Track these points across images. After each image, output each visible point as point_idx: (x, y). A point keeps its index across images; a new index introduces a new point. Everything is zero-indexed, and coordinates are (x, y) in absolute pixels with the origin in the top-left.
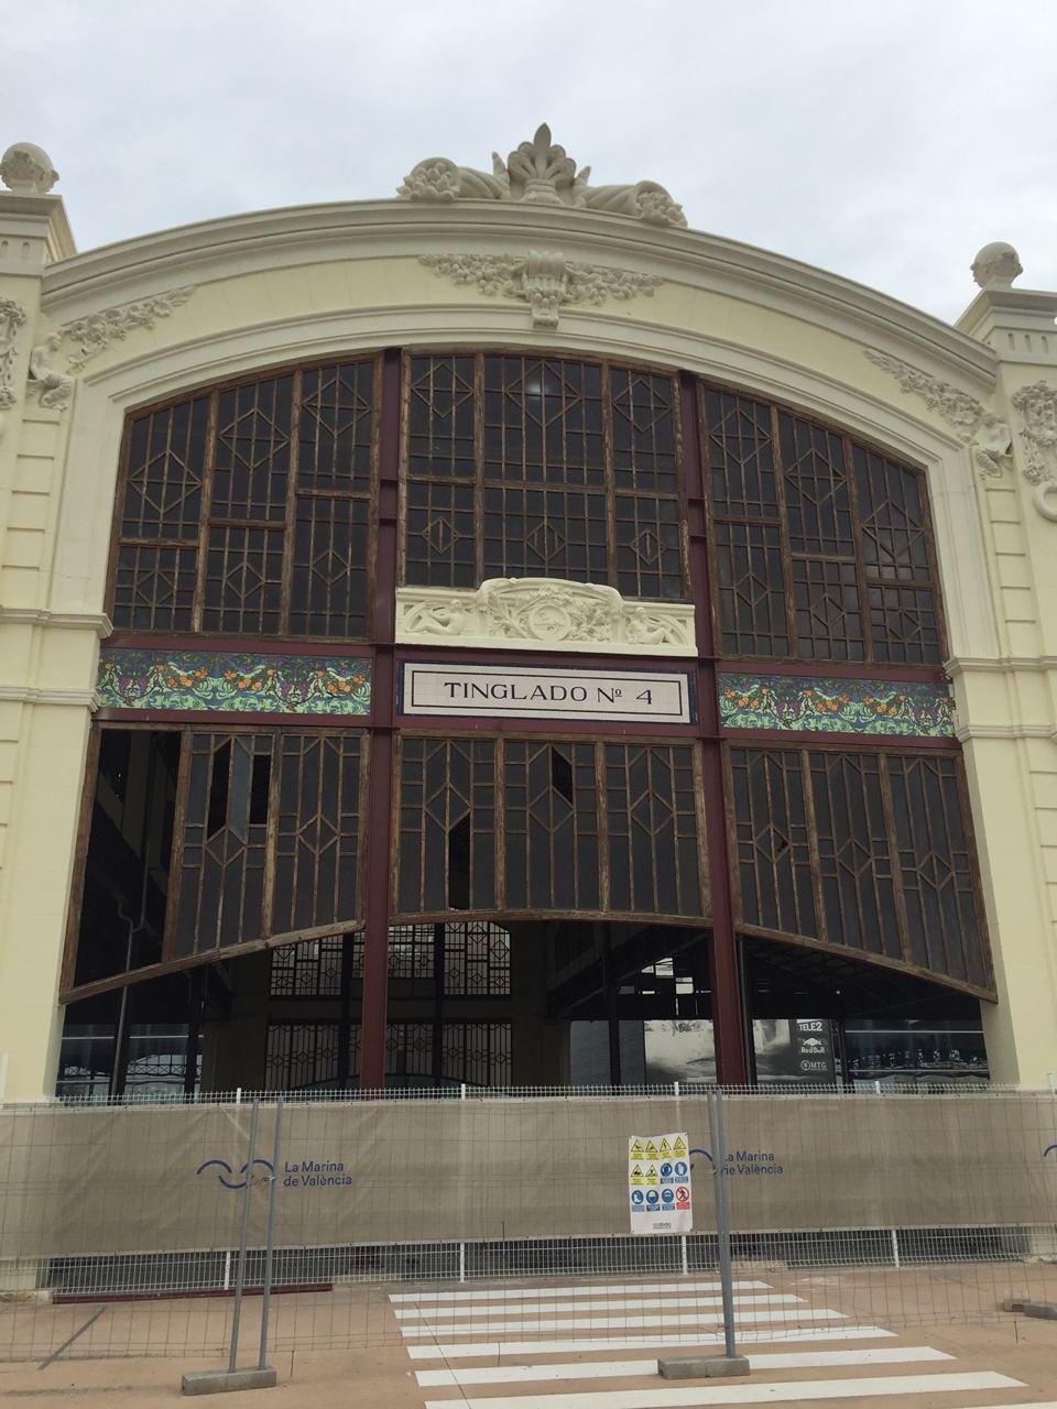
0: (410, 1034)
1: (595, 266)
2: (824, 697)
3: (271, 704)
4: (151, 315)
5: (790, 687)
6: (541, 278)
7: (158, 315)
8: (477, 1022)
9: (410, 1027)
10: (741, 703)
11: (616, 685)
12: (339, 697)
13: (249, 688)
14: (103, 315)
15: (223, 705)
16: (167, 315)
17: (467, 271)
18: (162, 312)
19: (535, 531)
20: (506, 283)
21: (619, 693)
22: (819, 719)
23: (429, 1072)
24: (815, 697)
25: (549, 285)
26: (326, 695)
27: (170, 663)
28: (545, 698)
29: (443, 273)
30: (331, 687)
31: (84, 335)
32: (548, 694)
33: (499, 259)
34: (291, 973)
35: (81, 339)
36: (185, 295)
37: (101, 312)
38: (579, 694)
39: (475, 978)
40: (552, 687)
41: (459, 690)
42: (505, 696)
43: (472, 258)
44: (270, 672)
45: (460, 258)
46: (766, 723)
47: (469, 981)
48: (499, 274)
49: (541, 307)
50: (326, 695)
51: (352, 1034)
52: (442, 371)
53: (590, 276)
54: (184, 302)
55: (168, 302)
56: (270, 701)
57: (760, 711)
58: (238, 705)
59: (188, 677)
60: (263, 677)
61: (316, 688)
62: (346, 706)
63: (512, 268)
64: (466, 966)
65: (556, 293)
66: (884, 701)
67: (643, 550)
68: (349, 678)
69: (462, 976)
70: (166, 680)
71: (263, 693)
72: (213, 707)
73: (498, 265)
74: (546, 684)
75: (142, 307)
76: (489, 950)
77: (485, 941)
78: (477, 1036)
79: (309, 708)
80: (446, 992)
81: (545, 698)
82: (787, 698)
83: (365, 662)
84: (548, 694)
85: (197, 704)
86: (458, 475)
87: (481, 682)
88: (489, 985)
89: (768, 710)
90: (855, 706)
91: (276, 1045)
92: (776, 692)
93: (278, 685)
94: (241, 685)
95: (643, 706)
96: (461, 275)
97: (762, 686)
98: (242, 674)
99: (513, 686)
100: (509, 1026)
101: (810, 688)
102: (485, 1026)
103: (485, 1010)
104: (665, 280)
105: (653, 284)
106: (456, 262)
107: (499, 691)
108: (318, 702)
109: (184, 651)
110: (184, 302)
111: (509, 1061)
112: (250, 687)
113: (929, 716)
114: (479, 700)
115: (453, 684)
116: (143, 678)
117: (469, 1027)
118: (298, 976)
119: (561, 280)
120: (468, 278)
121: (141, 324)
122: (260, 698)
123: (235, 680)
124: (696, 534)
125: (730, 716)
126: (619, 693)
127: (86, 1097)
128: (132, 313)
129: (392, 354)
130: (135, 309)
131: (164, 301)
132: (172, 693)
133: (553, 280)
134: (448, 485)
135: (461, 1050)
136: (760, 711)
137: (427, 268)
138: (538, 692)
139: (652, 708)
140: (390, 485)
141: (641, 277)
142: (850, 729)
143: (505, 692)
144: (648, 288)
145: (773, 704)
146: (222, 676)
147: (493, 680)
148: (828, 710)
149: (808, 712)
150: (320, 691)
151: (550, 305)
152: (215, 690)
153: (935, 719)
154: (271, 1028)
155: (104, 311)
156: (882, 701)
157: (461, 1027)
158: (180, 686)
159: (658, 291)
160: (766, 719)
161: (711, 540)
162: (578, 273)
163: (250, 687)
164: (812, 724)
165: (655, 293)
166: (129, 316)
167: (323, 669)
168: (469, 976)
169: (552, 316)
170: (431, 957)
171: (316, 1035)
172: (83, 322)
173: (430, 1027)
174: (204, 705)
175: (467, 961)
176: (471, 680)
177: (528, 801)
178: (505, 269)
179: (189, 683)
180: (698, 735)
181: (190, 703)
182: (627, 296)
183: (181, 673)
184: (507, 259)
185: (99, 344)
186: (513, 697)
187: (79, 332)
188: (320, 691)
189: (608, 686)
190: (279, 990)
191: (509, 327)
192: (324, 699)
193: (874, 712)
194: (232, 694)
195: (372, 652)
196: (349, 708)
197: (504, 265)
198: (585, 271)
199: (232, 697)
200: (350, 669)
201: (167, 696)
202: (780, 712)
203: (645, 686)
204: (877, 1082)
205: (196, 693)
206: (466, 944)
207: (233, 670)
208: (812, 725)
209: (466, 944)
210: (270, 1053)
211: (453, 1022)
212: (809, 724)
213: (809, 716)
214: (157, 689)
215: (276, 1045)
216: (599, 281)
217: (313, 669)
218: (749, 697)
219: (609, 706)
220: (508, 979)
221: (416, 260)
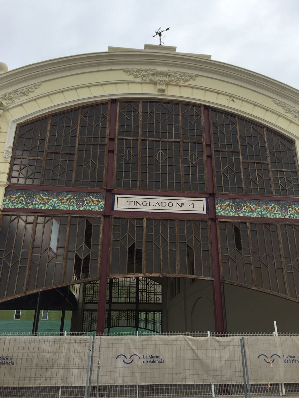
2: (250, 206)
3: (21, 206)
4: (28, 92)
5: (284, 205)
6: (160, 77)
7: (30, 92)
8: (150, 311)
9: (129, 312)
10: (12, 200)
13: (271, 210)
14: (13, 92)
15: (265, 216)
16: (33, 92)
18: (31, 91)
20: (150, 77)
21: (183, 204)
23: (134, 326)
25: (163, 78)
28: (160, 206)
30: (294, 211)
31: (7, 98)
32: (160, 205)
33: (148, 70)
35: (6, 100)
36: (39, 85)
37: (12, 91)
38: (170, 205)
39: (149, 298)
40: (162, 202)
42: (147, 205)
43: (139, 69)
45: (135, 70)
47: (148, 299)
48: (148, 75)
49: (160, 85)
50: (248, 211)
51: (112, 314)
52: (128, 104)
53: (176, 75)
55: (33, 88)
56: (72, 206)
58: (62, 208)
59: (97, 201)
60: (229, 205)
62: (46, 206)
63: (152, 73)
65: (165, 81)
68: (253, 206)
69: (145, 297)
71: (18, 202)
72: (54, 208)
76: (154, 289)
77: (153, 286)
78: (150, 315)
80: (140, 302)
81: (160, 206)
82: (284, 208)
84: (160, 205)
85: (49, 207)
88: (154, 300)
89: (232, 210)
91: (87, 317)
92: (280, 206)
94: (63, 201)
95: (191, 208)
98: (12, 196)
99: (149, 202)
100: (161, 313)
102: (153, 313)
103: (151, 307)
105: (195, 77)
106: (134, 71)
107: (145, 204)
108: (246, 213)
110: (39, 87)
111: (161, 323)
113: (81, 204)
114: (138, 206)
115: (130, 201)
117: (155, 313)
118: (94, 296)
121: (25, 95)
122: (17, 204)
123: (266, 208)
125: (265, 214)
127: (35, 333)
128: (22, 91)
129: (114, 101)
130: (23, 90)
132: (91, 206)
133: (164, 77)
134: (146, 140)
136: (229, 210)
137: (125, 73)
138: (157, 204)
139: (194, 209)
140: (112, 140)
142: (51, 208)
143: (147, 204)
145: (75, 201)
147: (142, 200)
149: (245, 211)
151: (163, 85)
152: (55, 203)
154: (85, 312)
155: (13, 91)
157: (145, 313)
159: (197, 79)
160: (277, 215)
163: (66, 202)
165: (196, 80)
166: (21, 92)
169: (164, 87)
170: (135, 291)
171: (92, 315)
172: (7, 94)
173: (135, 312)
174: (101, 209)
175: (147, 293)
178: (149, 73)
179: (97, 203)
181: (47, 207)
182: (187, 81)
183: (251, 206)
184: (150, 70)
186: (149, 206)
187: (5, 97)
189: (179, 202)
190: (115, 301)
191: (147, 91)
194: (8, 202)
195: (105, 191)
196: (97, 209)
197: (149, 72)
198: (174, 73)
199: (60, 205)
201: (90, 206)
203: (191, 202)
204: (43, 311)
206: (146, 287)
207: (220, 203)
208: (292, 217)
209: (146, 287)
210: (84, 319)
211: (142, 311)
212: (291, 216)
214: (36, 202)
215: (87, 317)
216: (178, 76)
217: (86, 196)
218: (226, 206)
219: (180, 208)
220: (161, 298)
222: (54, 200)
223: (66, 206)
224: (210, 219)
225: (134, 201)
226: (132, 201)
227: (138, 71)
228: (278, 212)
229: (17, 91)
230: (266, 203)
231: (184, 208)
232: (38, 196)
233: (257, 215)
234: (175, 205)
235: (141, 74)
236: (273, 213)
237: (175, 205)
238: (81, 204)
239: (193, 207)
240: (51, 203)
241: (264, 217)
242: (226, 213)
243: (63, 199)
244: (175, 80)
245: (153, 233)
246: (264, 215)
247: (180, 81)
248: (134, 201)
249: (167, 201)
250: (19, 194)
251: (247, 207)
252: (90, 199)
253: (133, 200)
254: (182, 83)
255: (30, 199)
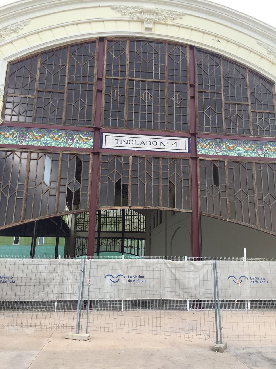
0: (108, 241)
1: (165, 10)
4: (18, 29)
6: (148, 14)
7: (20, 29)
8: (135, 239)
10: (6, 136)
11: (166, 141)
12: (36, 140)
13: (248, 150)
14: (3, 29)
16: (22, 29)
17: (125, 11)
18: (21, 28)
19: (143, 94)
20: (137, 15)
21: (167, 143)
22: (269, 154)
24: (268, 148)
26: (32, 140)
27: (33, 132)
28: (145, 144)
29: (118, 12)
30: (269, 150)
32: (146, 143)
33: (135, 8)
34: (83, 225)
40: (147, 141)
41: (119, 142)
42: (133, 144)
43: (127, 7)
44: (63, 135)
45: (123, 7)
46: (211, 153)
48: (135, 12)
49: (147, 23)
50: (226, 150)
52: (116, 43)
54: (28, 24)
55: (23, 25)
57: (209, 149)
58: (245, 155)
61: (29, 138)
62: (38, 143)
63: (139, 10)
64: (132, 224)
65: (152, 19)
66: (247, 147)
67: (176, 100)
69: (130, 227)
70: (268, 149)
71: (13, 139)
73: (135, 9)
74: (145, 140)
75: (15, 26)
76: (139, 220)
78: (135, 242)
79: (75, 146)
81: (145, 144)
83: (92, 132)
84: (146, 143)
85: (88, 147)
86: (136, 77)
87: (126, 139)
88: (138, 229)
90: (239, 148)
92: (19, 132)
93: (65, 139)
96: (123, 12)
97: (211, 142)
98: (245, 146)
100: (144, 240)
101: (267, 145)
102: (137, 240)
104: (186, 14)
105: (182, 15)
106: (122, 8)
107: (131, 142)
109: (84, 131)
110: (28, 24)
111: (144, 249)
112: (206, 147)
114: (125, 144)
115: (117, 140)
116: (220, 147)
117: (139, 240)
119: (154, 15)
120: (126, 13)
121: (15, 32)
122: (12, 140)
123: (244, 148)
124: (193, 95)
126: (167, 143)
128: (12, 28)
129: (102, 39)
130: (12, 27)
131: (21, 24)
133: (151, 15)
134: (133, 80)
135: (137, 247)
137: (113, 10)
138: (143, 143)
140: (100, 79)
141: (178, 13)
142: (43, 145)
143: (133, 142)
144: (180, 17)
146: (49, 136)
147: (129, 139)
148: (272, 151)
150: (30, 139)
151: (150, 23)
152: (47, 140)
153: (25, 140)
156: (247, 147)
158: (230, 149)
160: (211, 152)
161: (197, 97)
162: (159, 12)
163: (206, 147)
164: (267, 156)
166: (11, 29)
167: (225, 143)
168: (132, 227)
170: (121, 221)
173: (121, 240)
174: (43, 144)
175: (132, 223)
176: (122, 138)
177: (168, 176)
178: (137, 11)
179: (86, 140)
180: (93, 151)
181: (39, 144)
184: (138, 7)
185: (2, 38)
186: (135, 144)
188: (30, 139)
189: (163, 141)
191: (135, 29)
192: (79, 144)
193: (202, 147)
194: (3, 139)
196: (86, 146)
197: (137, 9)
198: (161, 11)
200: (274, 145)
202: (257, 152)
205: (88, 143)
206: (132, 218)
211: (127, 238)
213: (29, 141)
214: (29, 139)
216: (166, 14)
221: (109, 8)
222: (46, 138)
223: (249, 153)
224: (191, 157)
225: (121, 140)
226: (119, 140)
227: (126, 8)
228: (63, 141)
229: (7, 28)
230: (243, 143)
231: (167, 147)
232: (31, 133)
233: (235, 154)
234: (159, 143)
235: (129, 12)
236: (10, 139)
237: (159, 143)
238: (24, 139)
239: (176, 146)
240: (43, 140)
241: (241, 156)
242: (206, 152)
243: (55, 137)
244: (162, 19)
245: (138, 170)
246: (241, 154)
247: (167, 19)
248: (121, 140)
249: (152, 140)
250: (13, 131)
251: (226, 146)
252: (80, 137)
253: (120, 138)
254: (169, 22)
255: (260, 149)
